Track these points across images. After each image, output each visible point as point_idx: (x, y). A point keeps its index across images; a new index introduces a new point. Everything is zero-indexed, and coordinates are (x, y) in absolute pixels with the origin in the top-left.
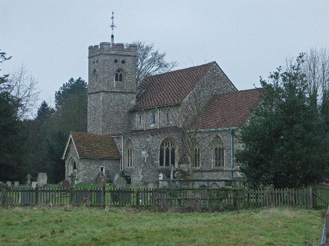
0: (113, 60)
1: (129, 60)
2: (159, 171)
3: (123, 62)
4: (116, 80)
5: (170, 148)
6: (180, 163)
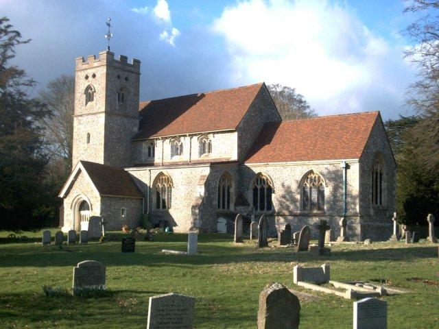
0: (117, 75)
1: (132, 77)
2: (219, 215)
3: (126, 79)
6: (237, 204)
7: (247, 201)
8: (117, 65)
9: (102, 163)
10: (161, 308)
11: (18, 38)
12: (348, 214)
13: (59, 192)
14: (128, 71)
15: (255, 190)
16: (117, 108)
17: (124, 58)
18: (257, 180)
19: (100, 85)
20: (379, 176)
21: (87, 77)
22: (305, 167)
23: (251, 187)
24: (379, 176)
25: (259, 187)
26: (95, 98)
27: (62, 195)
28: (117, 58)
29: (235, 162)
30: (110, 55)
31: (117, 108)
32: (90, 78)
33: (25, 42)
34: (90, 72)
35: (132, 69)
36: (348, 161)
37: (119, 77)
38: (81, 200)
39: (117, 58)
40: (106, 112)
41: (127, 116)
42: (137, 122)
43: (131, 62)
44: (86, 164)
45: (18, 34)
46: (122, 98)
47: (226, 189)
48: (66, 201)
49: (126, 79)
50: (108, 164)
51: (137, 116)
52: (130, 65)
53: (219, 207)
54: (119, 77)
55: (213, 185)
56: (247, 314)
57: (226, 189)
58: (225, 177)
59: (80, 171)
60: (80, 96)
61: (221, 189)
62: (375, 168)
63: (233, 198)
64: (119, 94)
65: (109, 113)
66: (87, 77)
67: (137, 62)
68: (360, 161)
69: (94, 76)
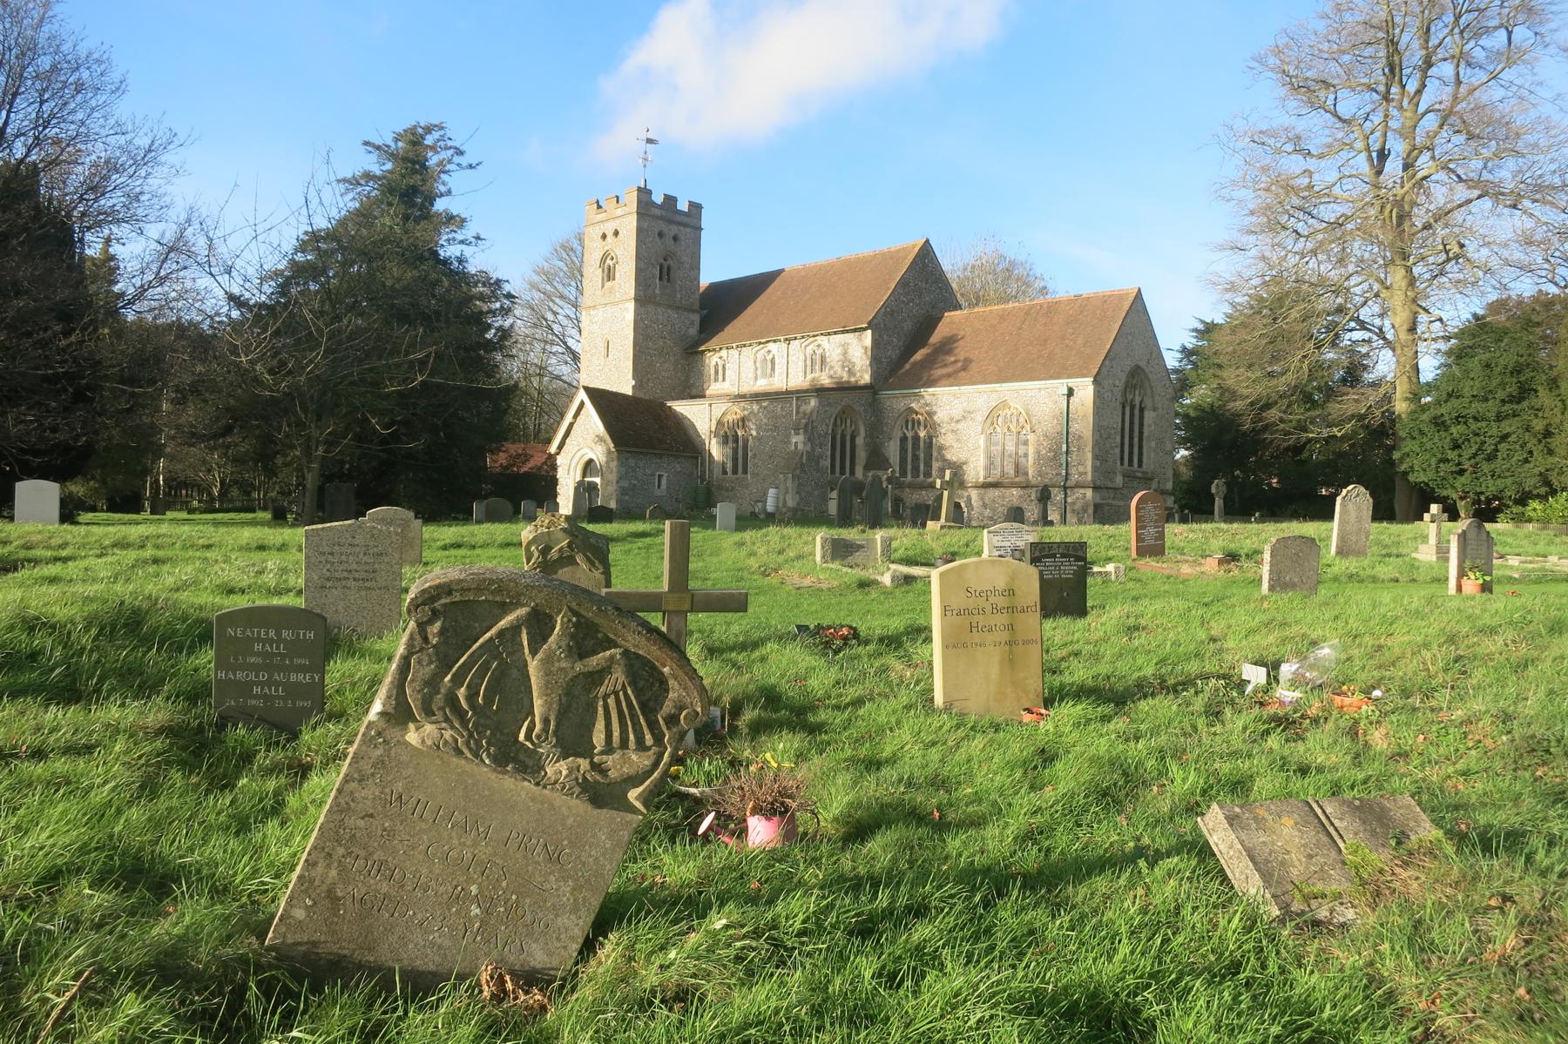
4: (661, 279)
5: (849, 432)
6: (867, 468)
7: (887, 461)
8: (657, 212)
9: (629, 392)
10: (327, 549)
11: (457, 159)
12: (1068, 485)
13: (549, 441)
14: (680, 224)
15: (904, 439)
16: (657, 291)
17: (670, 200)
18: (907, 422)
19: (626, 253)
20: (1137, 412)
21: (604, 237)
22: (994, 395)
23: (897, 434)
24: (1137, 412)
25: (910, 434)
26: (617, 275)
27: (553, 449)
28: (658, 198)
29: (865, 387)
30: (644, 193)
31: (657, 291)
32: (610, 237)
33: (471, 166)
34: (609, 228)
35: (685, 220)
36: (1072, 382)
37: (661, 235)
38: (586, 458)
39: (658, 198)
40: (636, 300)
41: (677, 308)
42: (696, 318)
43: (683, 206)
44: (590, 391)
45: (460, 153)
46: (666, 274)
47: (848, 438)
48: (560, 460)
49: (675, 239)
50: (641, 395)
51: (696, 306)
52: (681, 212)
53: (833, 472)
54: (661, 235)
55: (821, 429)
56: (1502, 815)
57: (848, 438)
58: (844, 415)
59: (582, 404)
60: (592, 273)
61: (839, 437)
62: (1130, 397)
63: (862, 455)
64: (661, 267)
65: (642, 300)
66: (604, 237)
67: (696, 208)
68: (1096, 382)
69: (616, 233)
